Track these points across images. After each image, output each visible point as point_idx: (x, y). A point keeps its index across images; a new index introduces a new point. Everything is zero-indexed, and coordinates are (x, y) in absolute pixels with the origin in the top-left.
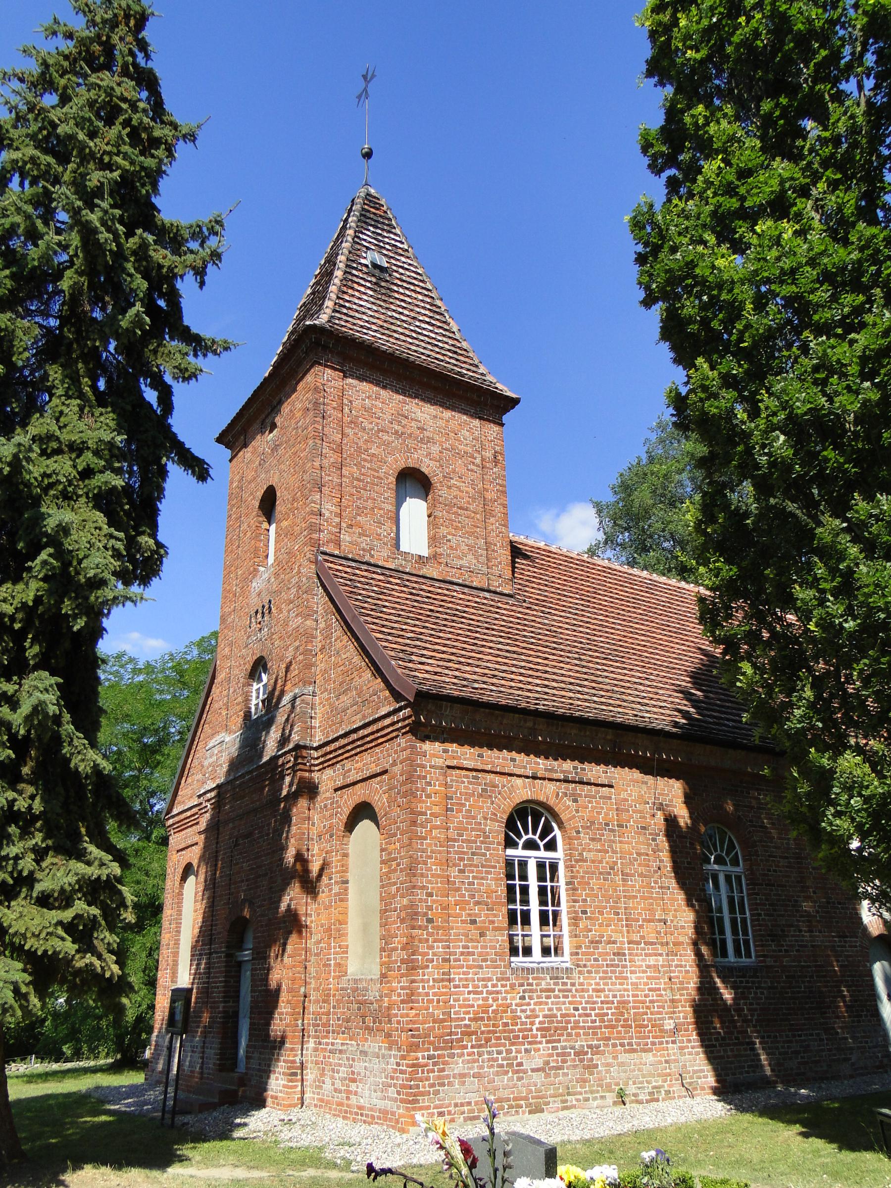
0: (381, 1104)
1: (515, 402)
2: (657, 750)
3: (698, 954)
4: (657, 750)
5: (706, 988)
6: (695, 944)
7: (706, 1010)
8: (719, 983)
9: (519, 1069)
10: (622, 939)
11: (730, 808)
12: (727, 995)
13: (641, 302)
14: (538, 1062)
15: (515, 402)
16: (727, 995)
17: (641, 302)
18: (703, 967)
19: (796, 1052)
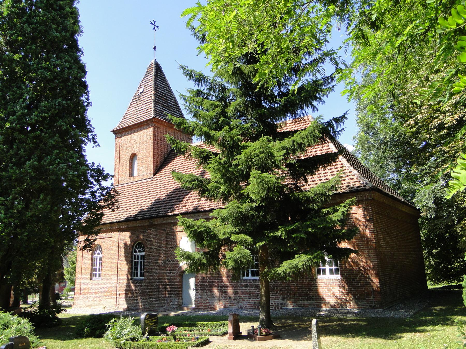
0: (354, 58)
1: (111, 131)
2: (120, 226)
3: (127, 277)
4: (120, 226)
5: (128, 285)
6: (127, 274)
7: (128, 290)
8: (132, 284)
9: (89, 300)
10: (110, 273)
11: (141, 237)
12: (133, 287)
13: (91, 105)
14: (92, 299)
15: (111, 131)
16: (133, 287)
17: (91, 105)
18: (128, 280)
19: (148, 303)
